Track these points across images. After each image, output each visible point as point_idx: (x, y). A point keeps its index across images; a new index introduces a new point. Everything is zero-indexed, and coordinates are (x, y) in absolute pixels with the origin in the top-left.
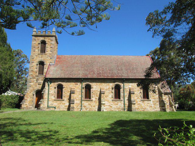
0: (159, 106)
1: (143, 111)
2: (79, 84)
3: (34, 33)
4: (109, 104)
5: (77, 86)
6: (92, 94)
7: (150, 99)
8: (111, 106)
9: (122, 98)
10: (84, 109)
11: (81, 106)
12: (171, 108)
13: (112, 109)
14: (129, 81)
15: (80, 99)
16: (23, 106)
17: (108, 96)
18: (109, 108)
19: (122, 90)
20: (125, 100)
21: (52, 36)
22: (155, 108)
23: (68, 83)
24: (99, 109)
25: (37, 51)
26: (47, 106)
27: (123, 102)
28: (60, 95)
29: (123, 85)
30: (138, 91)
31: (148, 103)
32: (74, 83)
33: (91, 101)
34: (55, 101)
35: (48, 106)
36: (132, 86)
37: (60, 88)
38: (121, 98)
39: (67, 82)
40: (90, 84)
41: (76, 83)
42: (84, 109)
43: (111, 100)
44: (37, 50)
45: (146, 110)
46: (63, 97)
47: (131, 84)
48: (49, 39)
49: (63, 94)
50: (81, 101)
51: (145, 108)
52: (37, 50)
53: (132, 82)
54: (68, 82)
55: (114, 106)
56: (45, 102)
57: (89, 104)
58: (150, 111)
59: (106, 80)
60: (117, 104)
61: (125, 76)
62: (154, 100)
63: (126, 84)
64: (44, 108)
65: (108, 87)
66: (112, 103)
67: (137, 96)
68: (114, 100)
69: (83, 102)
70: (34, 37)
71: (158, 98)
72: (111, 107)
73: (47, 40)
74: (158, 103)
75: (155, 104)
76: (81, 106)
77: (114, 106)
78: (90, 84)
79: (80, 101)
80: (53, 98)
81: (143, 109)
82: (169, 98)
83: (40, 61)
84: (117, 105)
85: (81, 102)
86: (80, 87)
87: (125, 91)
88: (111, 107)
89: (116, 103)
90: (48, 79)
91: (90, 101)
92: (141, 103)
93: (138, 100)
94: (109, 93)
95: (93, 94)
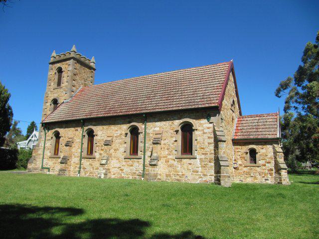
0: (213, 171)
1: (178, 180)
2: (79, 129)
3: (52, 60)
4: (118, 165)
5: (77, 133)
6: (95, 145)
7: (195, 153)
8: (122, 168)
9: (140, 154)
10: (83, 174)
11: (80, 168)
12: (277, 176)
13: (123, 175)
14: (155, 118)
15: (79, 154)
16: (30, 166)
17: (118, 150)
18: (119, 173)
19: (141, 137)
20: (146, 157)
21: (69, 59)
22: (205, 175)
23: (66, 129)
24: (218, 180)
25: (53, 85)
26: (41, 166)
27: (142, 160)
28: (187, 148)
29: (143, 126)
30: (172, 137)
31: (190, 164)
32: (73, 129)
33: (139, 159)
34: (50, 159)
35: (42, 166)
36: (160, 127)
37: (187, 130)
38: (139, 153)
39: (65, 128)
40: (191, 121)
41: (76, 128)
42: (83, 174)
43: (123, 157)
44: (52, 84)
45: (183, 180)
46: (94, 152)
47: (158, 124)
48: (67, 64)
49: (60, 148)
50: (81, 158)
51: (183, 175)
52: (52, 84)
53: (160, 120)
54: (67, 128)
55: (127, 169)
56: (38, 160)
57: (90, 164)
58: (193, 182)
59: (117, 119)
60: (132, 166)
61: (150, 108)
62: (203, 156)
63: (150, 125)
64: (36, 169)
65: (119, 132)
66: (124, 163)
67: (168, 149)
68: (129, 156)
69: (83, 161)
70: (51, 65)
71: (213, 152)
72: (121, 170)
73: (63, 66)
74: (213, 164)
75: (204, 167)
76: (80, 168)
77: (127, 169)
78: (191, 121)
79: (79, 159)
80: (48, 153)
81: (178, 177)
82: (275, 153)
83: (53, 100)
84: (131, 168)
85: (81, 160)
86: (81, 135)
87: (147, 139)
88: (121, 170)
89: (130, 162)
90: (82, 121)
91: (93, 159)
92: (175, 163)
93: (169, 157)
94: (121, 144)
95: (97, 146)
